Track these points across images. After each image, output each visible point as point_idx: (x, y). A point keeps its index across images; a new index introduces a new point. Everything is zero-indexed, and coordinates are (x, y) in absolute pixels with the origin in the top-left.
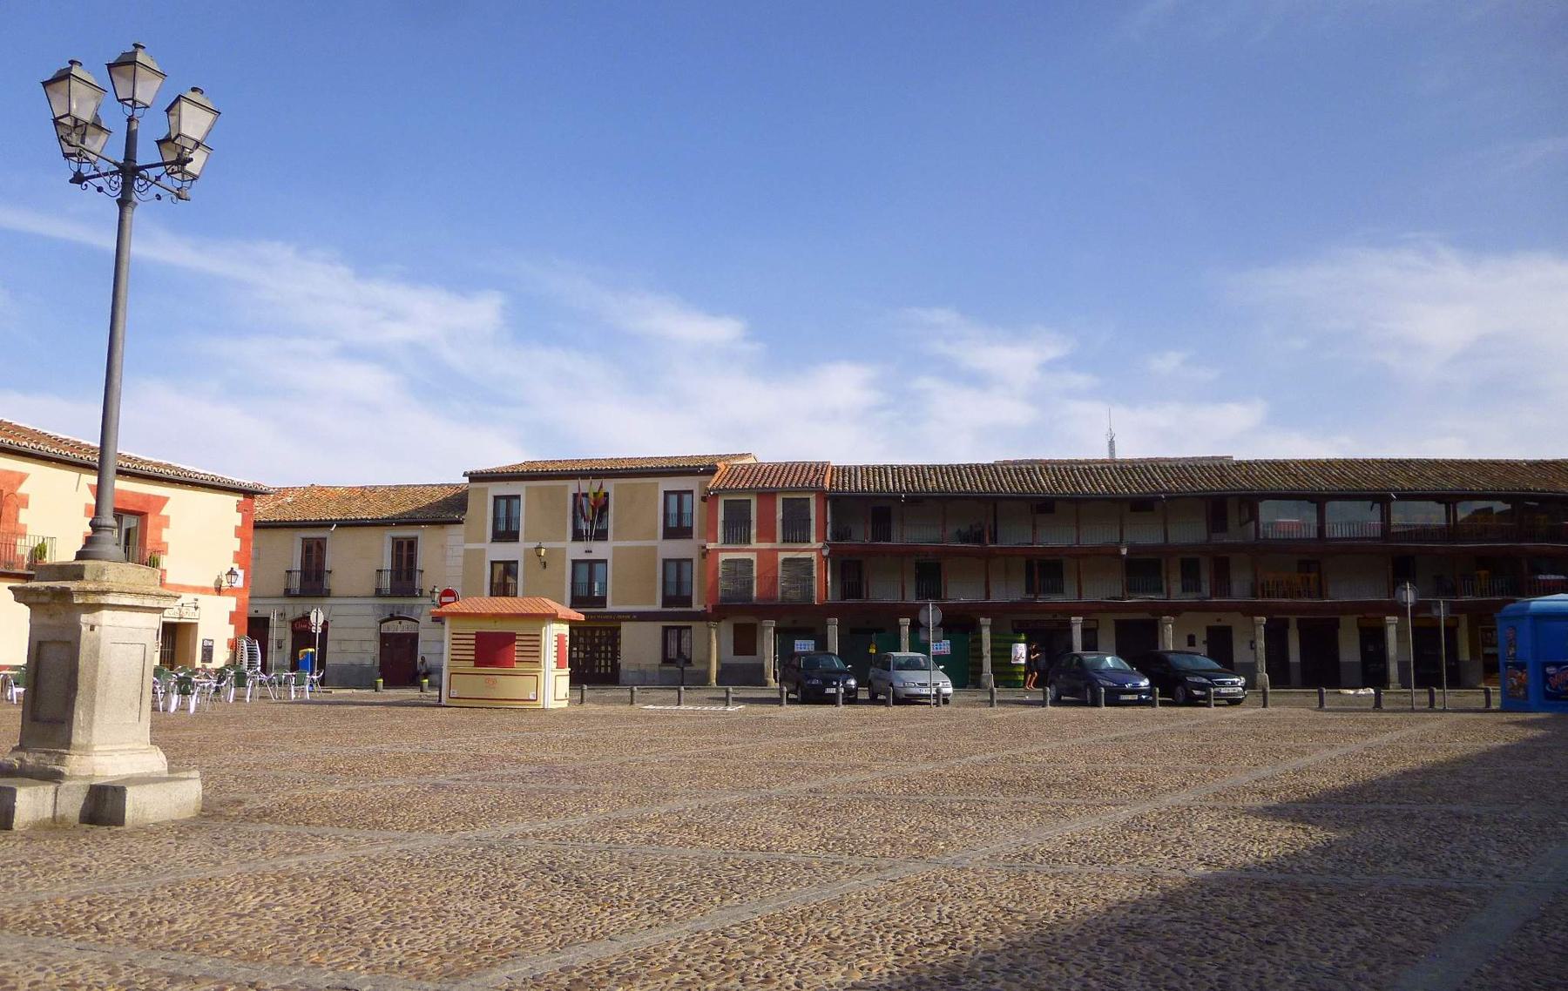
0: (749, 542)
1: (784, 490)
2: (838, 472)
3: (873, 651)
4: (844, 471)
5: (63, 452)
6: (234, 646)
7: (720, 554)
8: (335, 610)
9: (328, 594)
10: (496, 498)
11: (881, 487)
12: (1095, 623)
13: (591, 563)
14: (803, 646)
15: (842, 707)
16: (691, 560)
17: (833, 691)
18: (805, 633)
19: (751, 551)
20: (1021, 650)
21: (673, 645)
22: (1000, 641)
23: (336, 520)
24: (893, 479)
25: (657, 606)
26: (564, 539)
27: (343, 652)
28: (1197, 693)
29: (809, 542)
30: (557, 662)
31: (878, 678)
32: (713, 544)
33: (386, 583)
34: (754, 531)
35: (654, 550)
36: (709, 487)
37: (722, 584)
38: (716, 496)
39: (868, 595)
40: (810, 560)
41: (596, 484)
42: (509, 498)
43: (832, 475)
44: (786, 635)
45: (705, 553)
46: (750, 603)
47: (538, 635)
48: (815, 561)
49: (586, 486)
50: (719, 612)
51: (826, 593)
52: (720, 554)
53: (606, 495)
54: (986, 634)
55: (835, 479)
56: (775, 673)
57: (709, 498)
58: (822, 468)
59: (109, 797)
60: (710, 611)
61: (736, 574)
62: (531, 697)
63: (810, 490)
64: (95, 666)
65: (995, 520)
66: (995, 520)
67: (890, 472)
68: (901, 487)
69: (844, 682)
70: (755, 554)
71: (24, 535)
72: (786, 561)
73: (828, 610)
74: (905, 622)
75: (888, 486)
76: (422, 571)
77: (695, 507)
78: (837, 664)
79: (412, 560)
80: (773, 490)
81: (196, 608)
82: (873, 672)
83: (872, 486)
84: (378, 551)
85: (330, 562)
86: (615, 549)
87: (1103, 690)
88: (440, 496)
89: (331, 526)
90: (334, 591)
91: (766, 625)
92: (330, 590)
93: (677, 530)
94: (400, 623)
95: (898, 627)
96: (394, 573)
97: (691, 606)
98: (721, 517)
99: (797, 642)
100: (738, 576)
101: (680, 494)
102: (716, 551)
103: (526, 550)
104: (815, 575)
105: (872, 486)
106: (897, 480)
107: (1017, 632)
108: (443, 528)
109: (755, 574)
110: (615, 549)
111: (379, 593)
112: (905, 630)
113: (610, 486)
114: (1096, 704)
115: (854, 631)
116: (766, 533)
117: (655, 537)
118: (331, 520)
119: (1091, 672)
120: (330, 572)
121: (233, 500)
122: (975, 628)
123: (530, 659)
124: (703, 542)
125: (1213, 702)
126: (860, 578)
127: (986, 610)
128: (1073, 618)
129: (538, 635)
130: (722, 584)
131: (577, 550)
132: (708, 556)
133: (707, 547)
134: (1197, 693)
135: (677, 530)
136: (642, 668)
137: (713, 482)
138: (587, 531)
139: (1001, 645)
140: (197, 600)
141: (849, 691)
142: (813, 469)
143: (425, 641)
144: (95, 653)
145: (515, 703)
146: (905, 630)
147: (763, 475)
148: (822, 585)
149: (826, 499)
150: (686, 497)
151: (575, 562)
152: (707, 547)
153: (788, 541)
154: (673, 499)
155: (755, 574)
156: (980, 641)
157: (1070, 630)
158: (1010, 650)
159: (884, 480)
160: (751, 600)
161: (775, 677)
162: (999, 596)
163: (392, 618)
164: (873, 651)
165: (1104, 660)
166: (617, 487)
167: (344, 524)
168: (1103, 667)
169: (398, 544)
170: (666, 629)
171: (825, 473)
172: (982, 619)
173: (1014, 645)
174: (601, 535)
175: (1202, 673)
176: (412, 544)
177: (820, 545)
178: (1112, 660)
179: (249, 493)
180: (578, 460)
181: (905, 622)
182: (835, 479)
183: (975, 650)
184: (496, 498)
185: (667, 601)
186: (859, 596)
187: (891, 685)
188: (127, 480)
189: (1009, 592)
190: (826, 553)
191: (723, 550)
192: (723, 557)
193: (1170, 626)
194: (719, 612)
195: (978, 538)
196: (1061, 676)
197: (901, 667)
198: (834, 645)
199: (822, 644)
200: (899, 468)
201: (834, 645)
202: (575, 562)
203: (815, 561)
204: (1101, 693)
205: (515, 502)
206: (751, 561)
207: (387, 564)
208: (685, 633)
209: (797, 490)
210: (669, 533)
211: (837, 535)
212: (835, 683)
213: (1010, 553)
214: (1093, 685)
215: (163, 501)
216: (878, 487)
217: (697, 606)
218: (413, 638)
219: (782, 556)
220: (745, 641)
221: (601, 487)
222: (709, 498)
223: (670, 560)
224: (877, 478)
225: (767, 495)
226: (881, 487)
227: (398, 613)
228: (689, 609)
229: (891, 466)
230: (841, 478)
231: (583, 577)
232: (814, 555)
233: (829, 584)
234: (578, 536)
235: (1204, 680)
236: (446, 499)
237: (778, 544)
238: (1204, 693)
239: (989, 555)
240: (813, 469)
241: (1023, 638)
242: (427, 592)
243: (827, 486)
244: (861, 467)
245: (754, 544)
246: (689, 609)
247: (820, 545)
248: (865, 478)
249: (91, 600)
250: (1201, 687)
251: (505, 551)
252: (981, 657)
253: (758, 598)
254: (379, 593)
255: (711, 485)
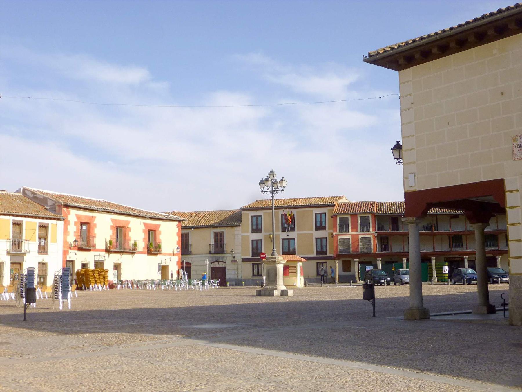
0: (348, 232)
1: (360, 213)
2: (378, 205)
3: (394, 269)
4: (381, 204)
5: (136, 213)
6: (178, 273)
7: (338, 236)
8: (194, 259)
9: (191, 253)
10: (252, 217)
11: (395, 211)
12: (474, 258)
13: (289, 239)
14: (369, 268)
15: (386, 286)
16: (326, 238)
17: (383, 281)
18: (369, 263)
19: (350, 234)
20: (446, 269)
21: (256, 269)
22: (438, 265)
23: (193, 226)
24: (399, 208)
25: (314, 255)
26: (279, 231)
27: (197, 274)
28: (495, 280)
29: (370, 231)
30: (301, 274)
31: (396, 278)
32: (335, 233)
33: (212, 249)
34: (350, 228)
35: (312, 234)
36: (334, 213)
37: (340, 247)
38: (336, 216)
39: (391, 250)
40: (370, 238)
41: (290, 210)
42: (257, 217)
43: (377, 207)
44: (362, 264)
45: (333, 236)
46: (349, 253)
47: (295, 266)
48: (372, 238)
49: (286, 211)
50: (338, 257)
51: (376, 249)
52: (338, 236)
53: (294, 215)
54: (434, 262)
55: (378, 208)
56: (359, 278)
57: (333, 217)
58: (373, 204)
59: (285, 292)
60: (335, 256)
61: (344, 244)
62: (294, 284)
63: (369, 213)
64: (279, 272)
65: (437, 222)
66: (437, 222)
67: (397, 204)
68: (402, 212)
69: (386, 279)
70: (351, 236)
71: (130, 240)
72: (362, 238)
73: (377, 255)
74: (405, 259)
75: (397, 211)
76: (226, 244)
77: (327, 219)
78: (383, 273)
79: (222, 240)
80: (356, 214)
81: (171, 261)
82: (395, 276)
83: (391, 211)
84: (209, 237)
85: (191, 242)
86: (298, 234)
87: (466, 279)
88: (227, 215)
89: (192, 228)
90: (193, 252)
91: (356, 261)
92: (191, 252)
93: (320, 227)
94: (218, 263)
95: (403, 261)
96: (215, 245)
97: (326, 254)
98: (338, 223)
99: (366, 267)
100: (345, 244)
101: (321, 214)
102: (337, 235)
103: (265, 236)
104: (372, 243)
105: (391, 211)
106: (400, 208)
107: (446, 262)
108: (233, 228)
109: (351, 243)
110: (298, 234)
111: (210, 253)
112: (405, 262)
113: (295, 211)
114: (464, 284)
115: (386, 262)
116: (355, 228)
117: (312, 230)
118: (191, 226)
119: (463, 274)
120: (191, 245)
121: (176, 223)
122: (430, 261)
123: (291, 273)
124: (331, 231)
125: (500, 283)
126: (388, 243)
127: (434, 254)
128: (464, 257)
129: (295, 266)
130: (340, 247)
131: (285, 235)
132: (334, 237)
133: (334, 234)
134: (495, 280)
135: (320, 227)
136: (310, 277)
137: (335, 210)
138: (287, 228)
139: (439, 267)
140: (171, 258)
141: (388, 281)
142: (369, 204)
143: (228, 269)
144: (279, 270)
145: (293, 286)
146: (405, 262)
147: (352, 207)
148: (375, 247)
149: (375, 216)
150: (323, 215)
151: (283, 239)
152: (334, 234)
153: (362, 231)
154: (318, 216)
155: (351, 243)
156: (431, 265)
157: (464, 261)
158: (442, 268)
159: (396, 208)
160: (350, 253)
161: (359, 279)
162: (438, 249)
163: (216, 261)
164: (394, 269)
165: (468, 271)
166: (297, 211)
167: (196, 228)
168: (468, 272)
169: (216, 234)
170: (318, 263)
171: (374, 206)
172: (432, 258)
173: (444, 267)
174: (293, 230)
175: (496, 274)
176: (221, 234)
177: (373, 232)
178: (471, 271)
179: (179, 221)
180: (277, 200)
181: (405, 259)
182: (378, 208)
183: (430, 268)
184: (252, 217)
185: (318, 253)
186: (388, 250)
187: (401, 279)
188: (115, 215)
189: (443, 247)
190: (376, 235)
191: (339, 235)
192: (339, 237)
193: (500, 259)
194: (338, 257)
195: (430, 228)
196: (458, 276)
197: (404, 274)
198: (379, 267)
199: (375, 267)
200: (401, 203)
201: (379, 267)
202: (283, 239)
203: (372, 238)
204: (465, 280)
205: (259, 218)
206: (349, 239)
207: (212, 242)
208: (324, 264)
209: (365, 213)
210: (318, 228)
211: (379, 229)
212: (383, 279)
213: (441, 234)
214: (463, 278)
215: (159, 226)
216: (394, 212)
217: (329, 255)
218: (224, 269)
219: (360, 237)
220: (347, 267)
221: (292, 212)
222: (333, 217)
223: (255, 216)
224: (393, 207)
225: (354, 215)
226: (395, 211)
227: (218, 260)
228: (326, 256)
229: (398, 202)
230: (380, 208)
231: (286, 244)
232: (371, 236)
233: (377, 246)
234: (284, 230)
235: (498, 276)
236: (230, 216)
237: (359, 232)
238: (497, 280)
239: (434, 235)
240: (369, 204)
241: (447, 264)
242: (229, 251)
243: (375, 211)
244: (387, 203)
245: (350, 232)
246: (326, 256)
247: (373, 232)
248: (389, 208)
249: (279, 262)
250: (497, 278)
251: (256, 236)
252: (432, 271)
253: (353, 251)
254: (210, 253)
255: (334, 212)
